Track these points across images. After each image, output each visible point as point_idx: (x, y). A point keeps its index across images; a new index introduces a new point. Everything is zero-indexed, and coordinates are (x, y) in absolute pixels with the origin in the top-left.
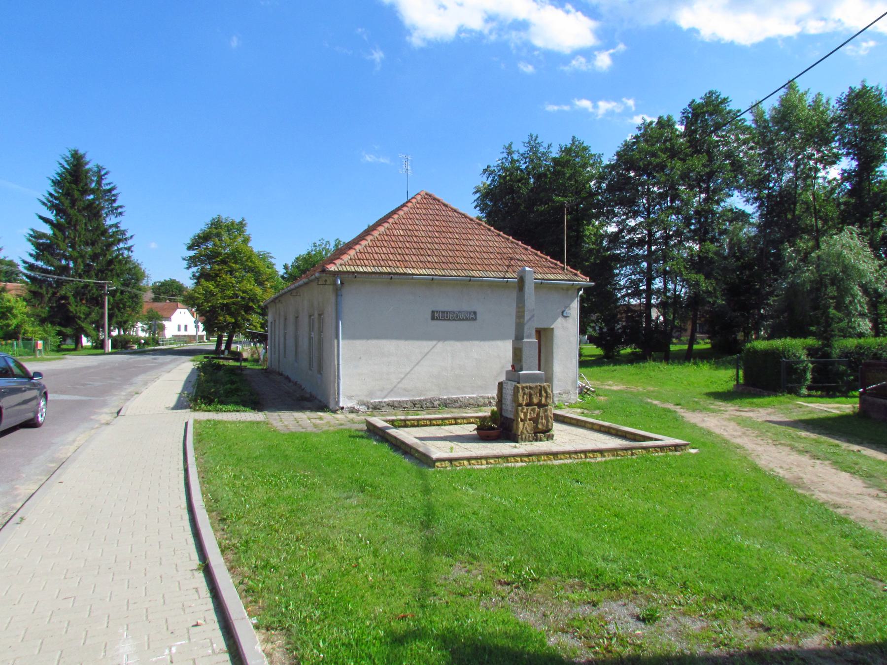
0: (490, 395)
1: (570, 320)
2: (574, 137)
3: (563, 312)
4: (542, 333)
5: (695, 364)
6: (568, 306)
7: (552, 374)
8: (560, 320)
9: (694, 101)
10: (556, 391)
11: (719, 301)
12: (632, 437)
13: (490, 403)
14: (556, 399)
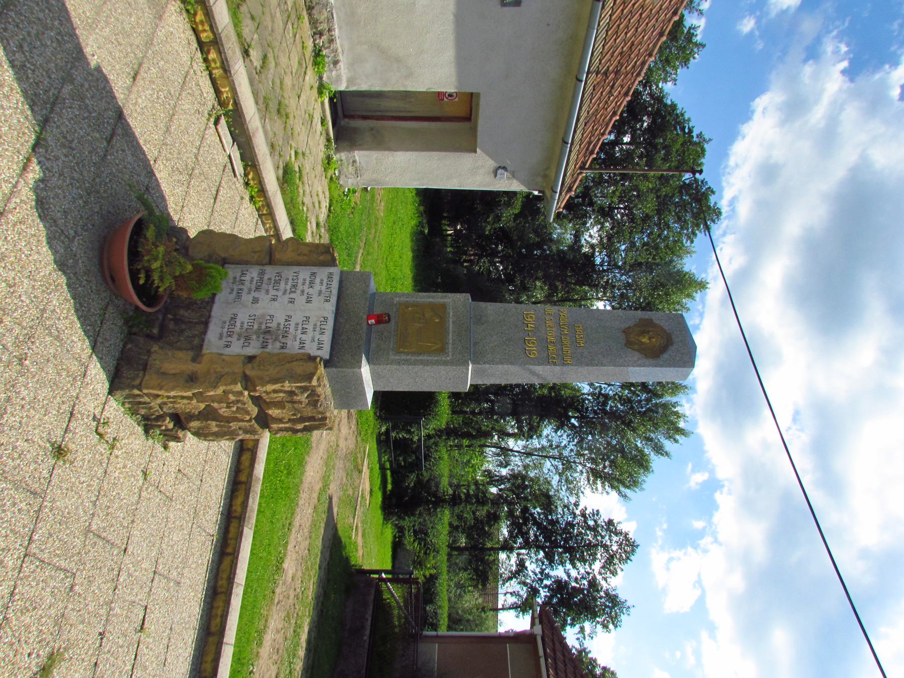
0: (336, 33)
1: (489, 178)
2: (703, 46)
3: (504, 168)
4: (466, 125)
5: (415, 201)
6: (514, 175)
7: (390, 149)
8: (491, 164)
9: (713, 192)
10: (358, 155)
11: (489, 228)
12: (237, 508)
13: (321, 34)
14: (343, 155)
